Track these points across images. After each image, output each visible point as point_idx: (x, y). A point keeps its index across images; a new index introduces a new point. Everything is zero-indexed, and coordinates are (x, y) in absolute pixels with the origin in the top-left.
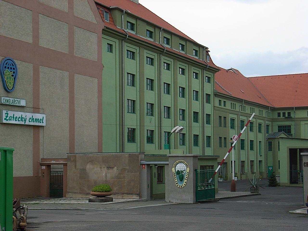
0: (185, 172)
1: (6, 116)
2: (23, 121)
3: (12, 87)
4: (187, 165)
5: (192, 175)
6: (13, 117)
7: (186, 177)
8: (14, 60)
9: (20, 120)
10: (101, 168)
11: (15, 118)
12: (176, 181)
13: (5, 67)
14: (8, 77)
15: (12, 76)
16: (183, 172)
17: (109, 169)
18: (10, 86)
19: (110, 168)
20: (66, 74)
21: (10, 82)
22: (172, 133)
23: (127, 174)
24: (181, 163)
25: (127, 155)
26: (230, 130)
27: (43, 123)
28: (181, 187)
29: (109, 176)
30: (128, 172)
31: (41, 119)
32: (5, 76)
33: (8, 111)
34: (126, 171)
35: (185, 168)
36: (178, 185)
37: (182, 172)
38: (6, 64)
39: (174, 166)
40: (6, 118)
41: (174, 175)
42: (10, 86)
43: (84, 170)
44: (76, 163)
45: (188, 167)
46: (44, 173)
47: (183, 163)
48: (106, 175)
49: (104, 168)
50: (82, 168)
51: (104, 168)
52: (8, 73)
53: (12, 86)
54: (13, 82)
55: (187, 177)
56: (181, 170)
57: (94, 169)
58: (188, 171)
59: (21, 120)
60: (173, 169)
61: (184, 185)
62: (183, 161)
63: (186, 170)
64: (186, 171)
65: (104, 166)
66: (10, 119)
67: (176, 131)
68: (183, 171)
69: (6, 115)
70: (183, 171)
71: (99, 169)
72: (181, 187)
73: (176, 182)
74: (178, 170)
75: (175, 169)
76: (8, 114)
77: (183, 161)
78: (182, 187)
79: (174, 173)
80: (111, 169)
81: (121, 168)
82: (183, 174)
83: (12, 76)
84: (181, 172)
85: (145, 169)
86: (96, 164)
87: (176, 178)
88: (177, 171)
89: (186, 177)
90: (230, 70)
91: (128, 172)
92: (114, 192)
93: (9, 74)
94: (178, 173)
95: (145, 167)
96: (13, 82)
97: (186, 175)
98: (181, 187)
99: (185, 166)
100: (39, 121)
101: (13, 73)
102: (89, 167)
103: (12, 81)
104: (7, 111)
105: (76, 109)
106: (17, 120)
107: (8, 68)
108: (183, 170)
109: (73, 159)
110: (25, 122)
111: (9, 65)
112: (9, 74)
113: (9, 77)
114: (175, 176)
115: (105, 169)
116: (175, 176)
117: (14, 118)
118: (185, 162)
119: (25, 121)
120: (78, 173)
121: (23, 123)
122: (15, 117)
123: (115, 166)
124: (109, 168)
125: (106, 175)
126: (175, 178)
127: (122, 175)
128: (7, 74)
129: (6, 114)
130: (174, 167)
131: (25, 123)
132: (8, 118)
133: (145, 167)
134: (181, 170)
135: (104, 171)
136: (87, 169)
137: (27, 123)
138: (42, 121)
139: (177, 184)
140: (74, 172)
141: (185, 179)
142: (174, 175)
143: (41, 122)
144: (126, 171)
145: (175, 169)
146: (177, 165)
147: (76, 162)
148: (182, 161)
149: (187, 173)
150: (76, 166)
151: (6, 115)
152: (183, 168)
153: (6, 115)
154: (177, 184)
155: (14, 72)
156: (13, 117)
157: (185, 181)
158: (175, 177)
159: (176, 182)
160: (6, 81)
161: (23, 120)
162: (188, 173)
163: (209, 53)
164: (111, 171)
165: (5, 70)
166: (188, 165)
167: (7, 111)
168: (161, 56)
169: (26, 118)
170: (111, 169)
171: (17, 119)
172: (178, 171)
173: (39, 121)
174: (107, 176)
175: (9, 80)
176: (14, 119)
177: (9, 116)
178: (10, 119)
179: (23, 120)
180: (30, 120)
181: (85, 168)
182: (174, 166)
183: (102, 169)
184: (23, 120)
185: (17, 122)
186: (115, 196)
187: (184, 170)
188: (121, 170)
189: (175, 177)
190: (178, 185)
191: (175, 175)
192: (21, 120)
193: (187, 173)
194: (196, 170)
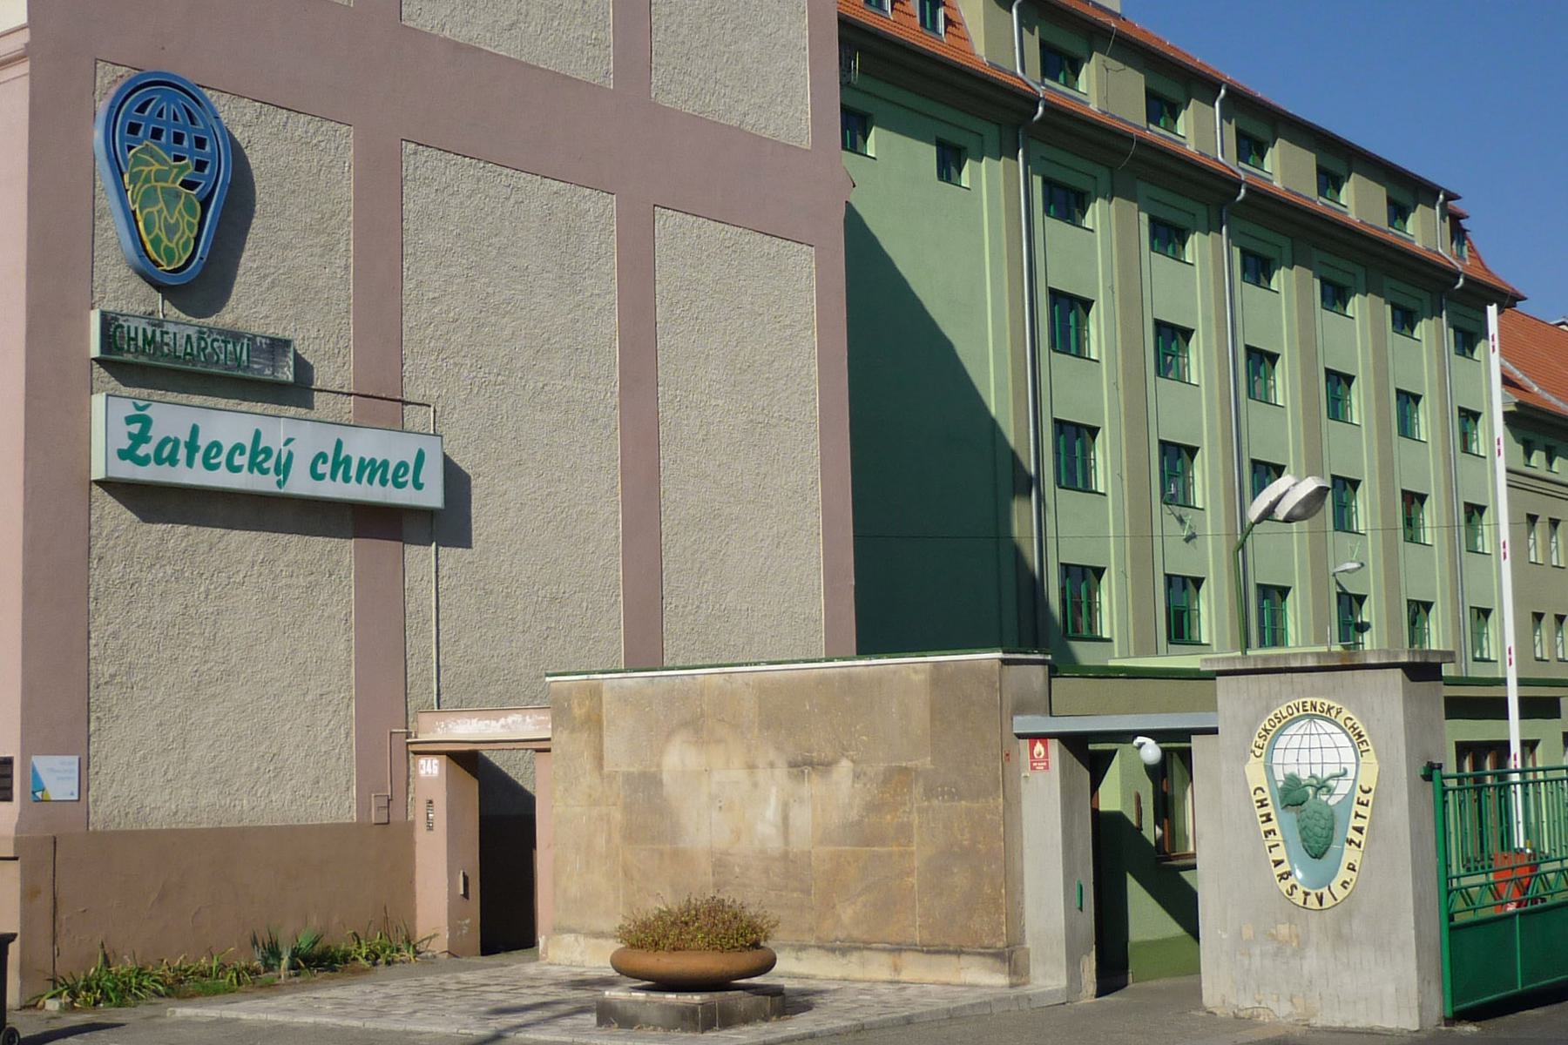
0: (1343, 787)
1: (131, 435)
2: (264, 472)
3: (185, 258)
4: (1360, 736)
5: (1399, 812)
6: (192, 447)
7: (1356, 829)
8: (208, 93)
9: (242, 466)
10: (751, 767)
11: (202, 452)
12: (1279, 853)
13: (134, 129)
14: (155, 189)
15: (189, 185)
16: (1330, 791)
17: (803, 772)
18: (173, 245)
19: (811, 764)
20: (600, 208)
21: (172, 222)
22: (1253, 525)
23: (920, 810)
24: (1312, 717)
25: (916, 672)
26: (1359, 862)
27: (418, 486)
28: (1316, 905)
29: (803, 819)
30: (930, 793)
31: (403, 464)
32: (133, 180)
33: (148, 406)
34: (918, 790)
35: (1349, 755)
36: (1294, 887)
37: (1322, 786)
38: (142, 109)
39: (1260, 742)
40: (134, 447)
41: (1264, 810)
42: (167, 247)
43: (648, 783)
44: (601, 737)
45: (1364, 747)
46: (431, 802)
47: (1326, 716)
48: (785, 818)
49: (772, 765)
50: (635, 769)
51: (772, 765)
52: (157, 166)
53: (185, 250)
54: (189, 223)
55: (1359, 830)
56: (1317, 771)
57: (708, 771)
58: (1369, 778)
59: (253, 465)
60: (1255, 773)
61: (1344, 884)
62: (1328, 703)
63: (1351, 775)
64: (1355, 780)
65: (772, 755)
66: (165, 454)
67: (1282, 512)
68: (1332, 777)
69: (135, 428)
70: (1332, 783)
71: (739, 774)
72: (1321, 904)
73: (1278, 863)
74: (1289, 770)
75: (1269, 770)
76: (146, 422)
77: (1328, 703)
78: (1328, 901)
79: (1260, 796)
80: (813, 776)
81: (882, 766)
82: (1331, 802)
83: (189, 185)
84: (1310, 791)
85: (1047, 768)
86: (719, 741)
87: (1279, 837)
88: (1280, 784)
89: (1356, 829)
90: (1562, 327)
91: (930, 793)
92: (842, 937)
93: (157, 171)
94: (1293, 795)
95: (1046, 756)
96: (196, 221)
97: (1356, 808)
98: (1321, 904)
99: (1342, 740)
100: (389, 476)
101: (192, 168)
102: (677, 758)
103: (187, 218)
104: (141, 403)
105: (666, 413)
106: (220, 463)
107: (156, 134)
108: (1326, 776)
109: (584, 710)
110: (285, 478)
111: (175, 118)
112: (161, 176)
113: (162, 188)
114: (1269, 820)
115: (781, 772)
116: (1269, 820)
117: (197, 449)
118: (1346, 713)
119: (284, 469)
120: (614, 804)
121: (265, 483)
122: (203, 442)
123: (844, 751)
124: (803, 766)
125: (785, 818)
126: (1267, 833)
127: (889, 817)
128: (147, 169)
129: (130, 420)
130: (1258, 752)
131: (279, 484)
132: (142, 451)
133: (1046, 756)
134: (1312, 776)
135: (775, 785)
136: (666, 777)
137: (300, 484)
138: (410, 476)
139: (1283, 877)
140: (590, 796)
141: (1351, 842)
142: (1264, 810)
143: (403, 485)
144: (918, 790)
145: (1269, 770)
146: (1279, 733)
147: (601, 728)
148: (1318, 701)
149: (1358, 793)
150: (599, 759)
151: (135, 428)
152: (1330, 755)
153: (136, 432)
154: (1283, 877)
155: (200, 166)
156: (187, 445)
157: (1351, 855)
158: (1268, 826)
159: (1278, 863)
160: (134, 212)
161: (270, 464)
162: (1370, 797)
163: (1461, 221)
164: (813, 787)
165: (130, 148)
166: (1368, 730)
167: (141, 403)
168: (1224, 214)
169: (290, 455)
170: (813, 776)
171: (223, 458)
172: (1293, 782)
173: (389, 476)
174: (791, 821)
175: (160, 212)
176: (199, 457)
177: (156, 434)
178: (165, 454)
179: (265, 465)
180: (325, 469)
181: (653, 769)
182: (1260, 742)
183: (762, 775)
184: (265, 465)
185: (221, 479)
186: (844, 962)
187: (1337, 771)
188: (881, 777)
189: (1268, 826)
190: (1294, 887)
191: (1269, 809)
192: (253, 465)
193: (1364, 798)
194: (1430, 772)
